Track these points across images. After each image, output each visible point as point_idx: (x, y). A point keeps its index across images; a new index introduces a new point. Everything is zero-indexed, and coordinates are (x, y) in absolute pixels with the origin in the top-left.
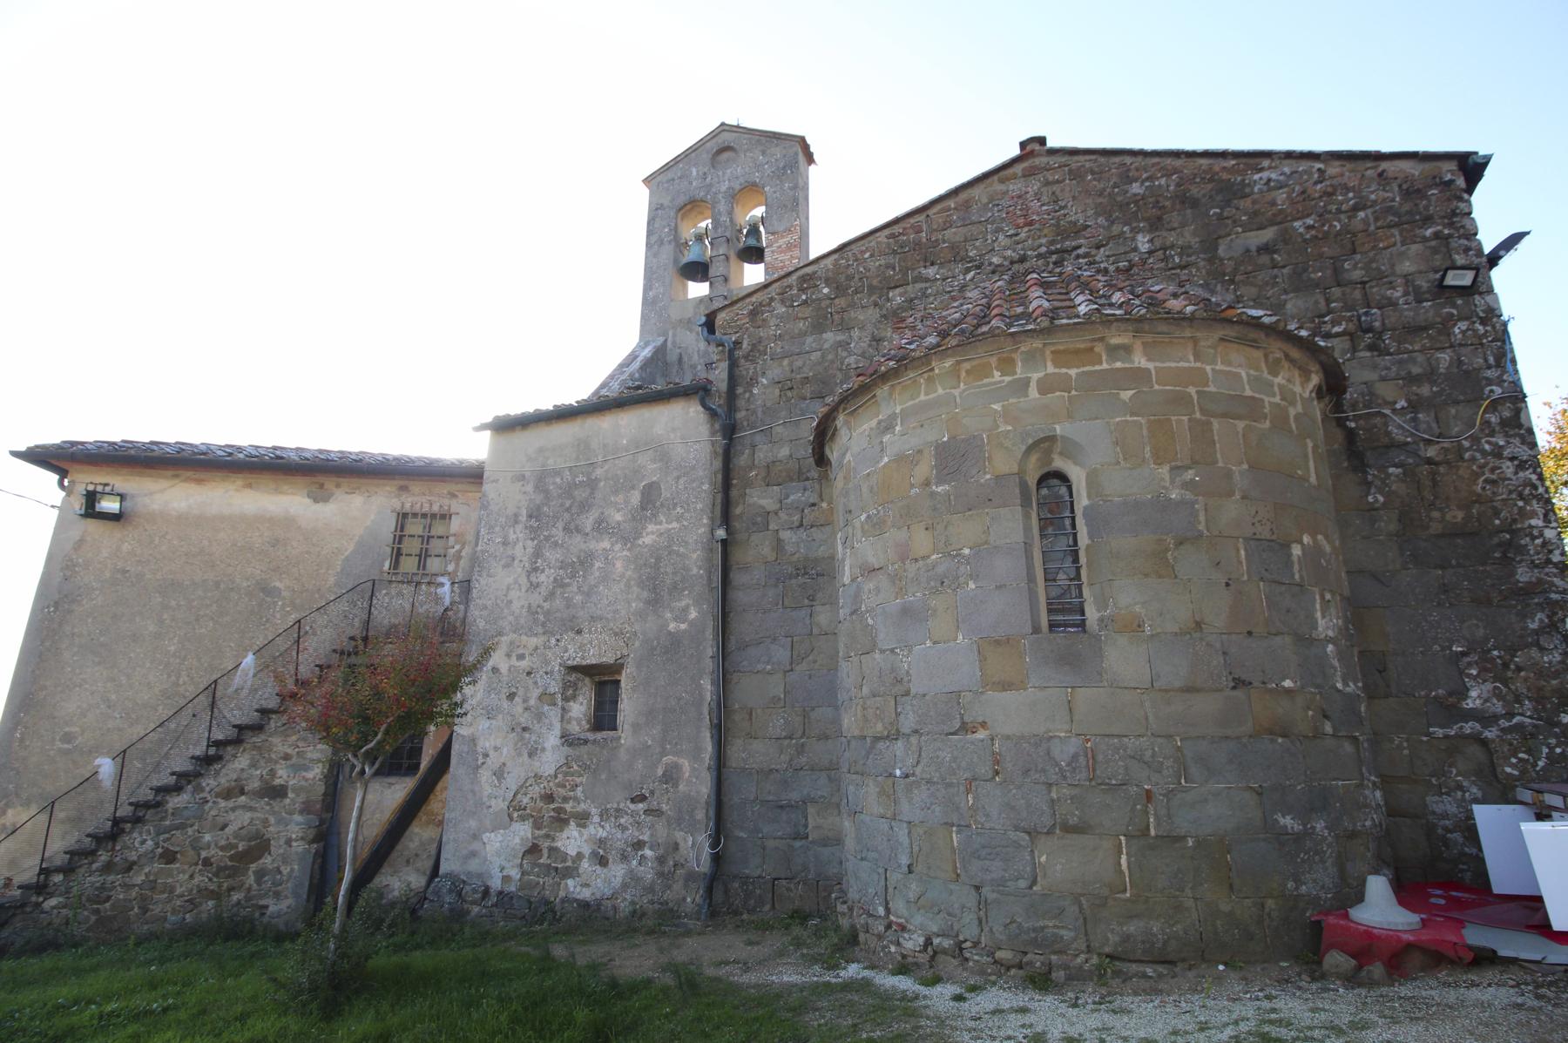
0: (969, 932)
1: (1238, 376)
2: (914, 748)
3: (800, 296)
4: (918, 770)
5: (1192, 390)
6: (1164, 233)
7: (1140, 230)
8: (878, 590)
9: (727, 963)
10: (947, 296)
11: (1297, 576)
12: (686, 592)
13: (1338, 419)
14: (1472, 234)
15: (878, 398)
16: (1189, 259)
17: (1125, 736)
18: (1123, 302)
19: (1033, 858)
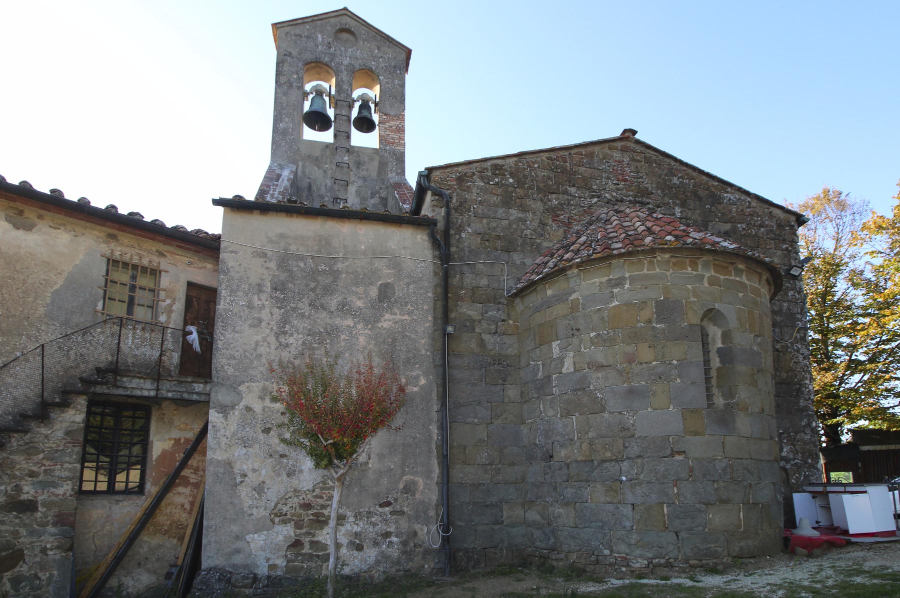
3: (494, 179)
4: (641, 477)
10: (582, 209)
12: (417, 366)
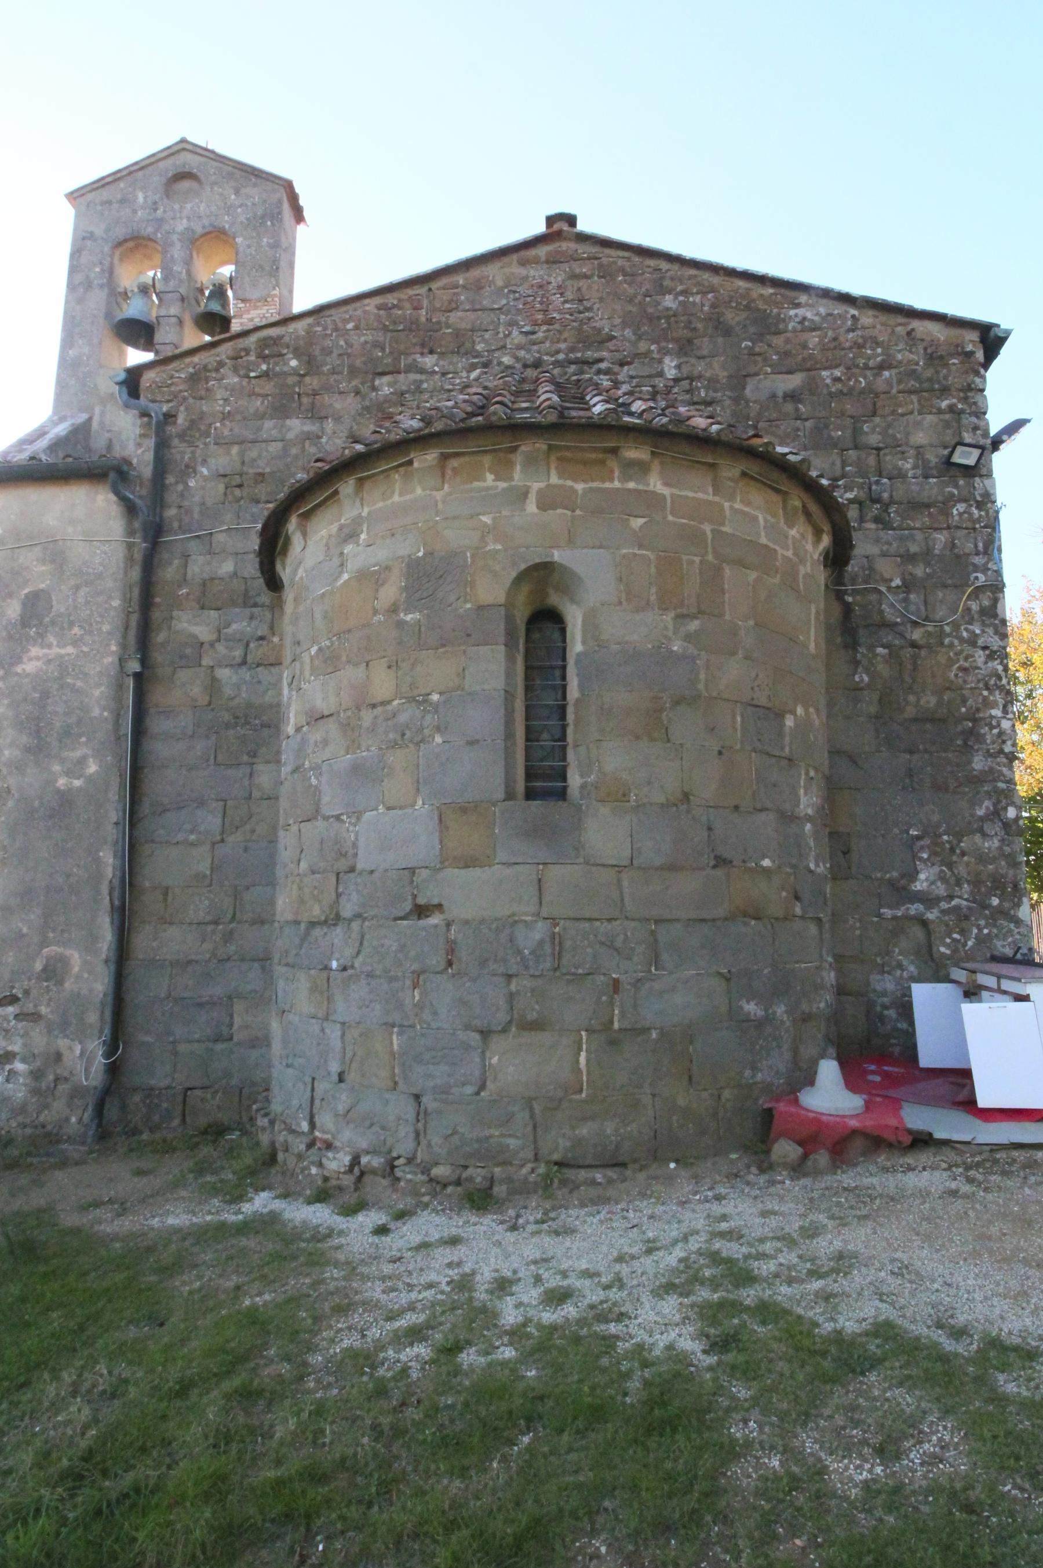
0: (404, 1147)
1: (755, 519)
5: (707, 528)
6: (693, 361)
7: (667, 352)
9: (97, 1204)
12: (83, 739)
14: (981, 413)
15: (341, 496)
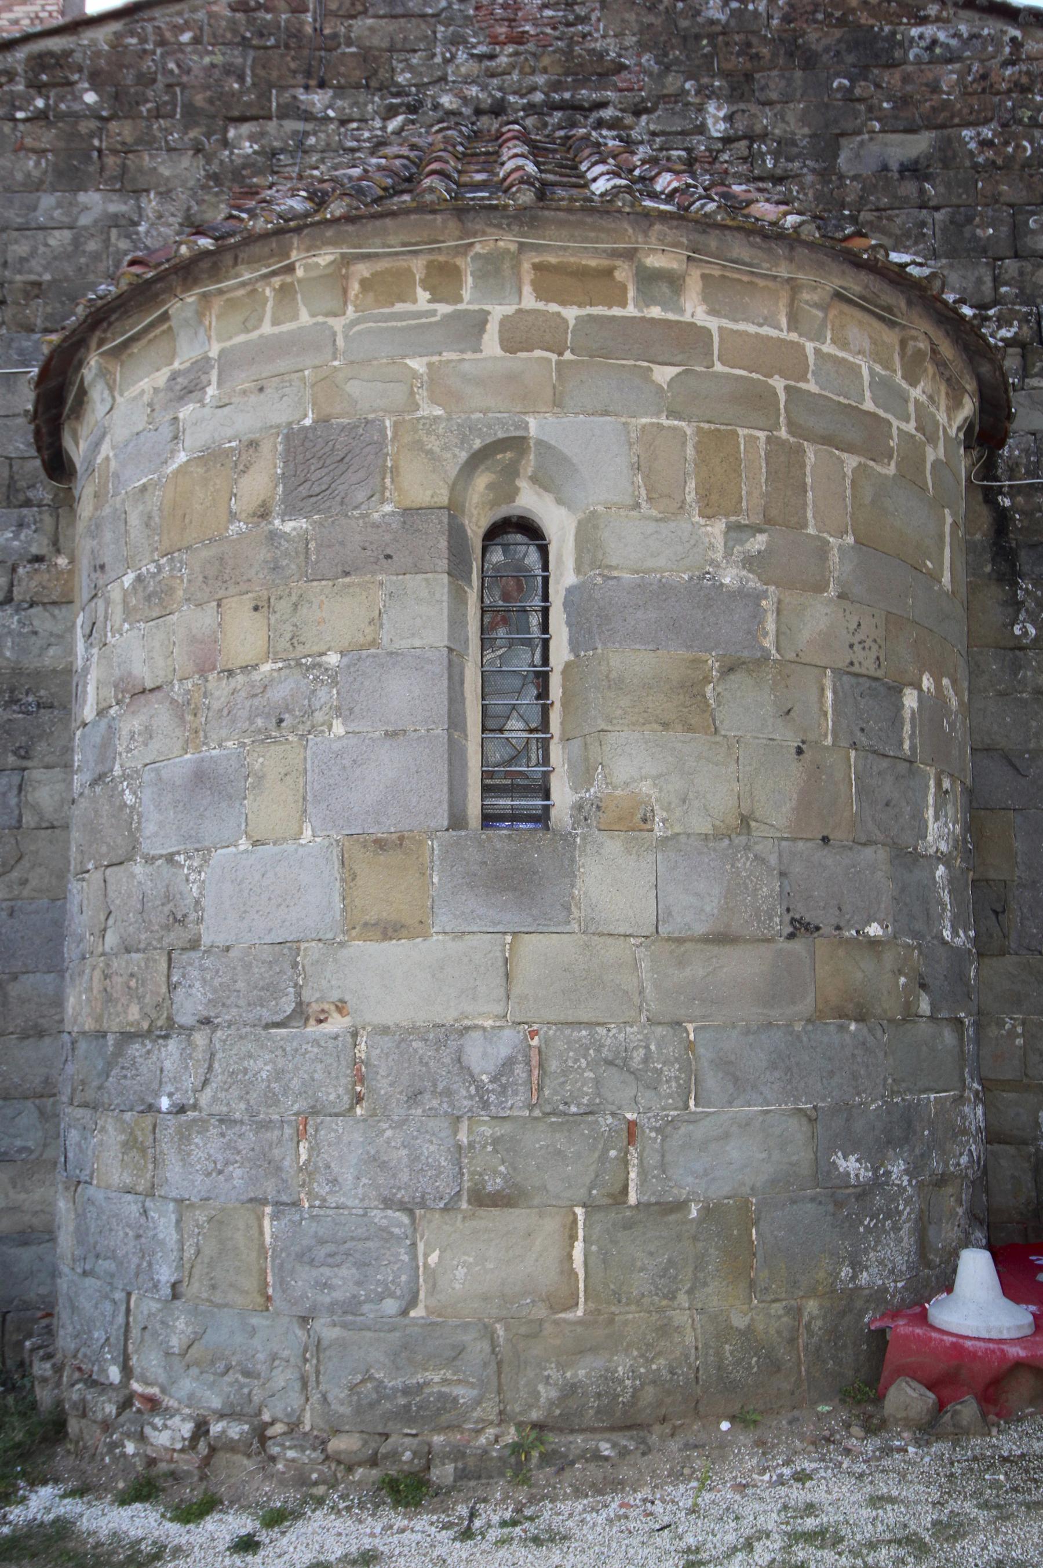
2: (199, 1055)
3: (30, 100)
4: (205, 1098)
5: (778, 383)
6: (754, 108)
8: (149, 733)
11: (906, 746)
13: (987, 491)
16: (790, 165)
17: (598, 1024)
18: (675, 190)
19: (414, 1257)
